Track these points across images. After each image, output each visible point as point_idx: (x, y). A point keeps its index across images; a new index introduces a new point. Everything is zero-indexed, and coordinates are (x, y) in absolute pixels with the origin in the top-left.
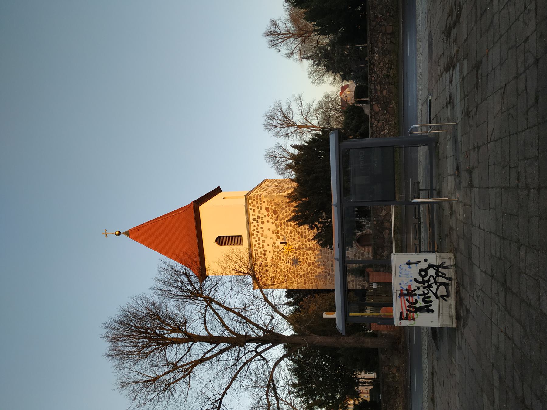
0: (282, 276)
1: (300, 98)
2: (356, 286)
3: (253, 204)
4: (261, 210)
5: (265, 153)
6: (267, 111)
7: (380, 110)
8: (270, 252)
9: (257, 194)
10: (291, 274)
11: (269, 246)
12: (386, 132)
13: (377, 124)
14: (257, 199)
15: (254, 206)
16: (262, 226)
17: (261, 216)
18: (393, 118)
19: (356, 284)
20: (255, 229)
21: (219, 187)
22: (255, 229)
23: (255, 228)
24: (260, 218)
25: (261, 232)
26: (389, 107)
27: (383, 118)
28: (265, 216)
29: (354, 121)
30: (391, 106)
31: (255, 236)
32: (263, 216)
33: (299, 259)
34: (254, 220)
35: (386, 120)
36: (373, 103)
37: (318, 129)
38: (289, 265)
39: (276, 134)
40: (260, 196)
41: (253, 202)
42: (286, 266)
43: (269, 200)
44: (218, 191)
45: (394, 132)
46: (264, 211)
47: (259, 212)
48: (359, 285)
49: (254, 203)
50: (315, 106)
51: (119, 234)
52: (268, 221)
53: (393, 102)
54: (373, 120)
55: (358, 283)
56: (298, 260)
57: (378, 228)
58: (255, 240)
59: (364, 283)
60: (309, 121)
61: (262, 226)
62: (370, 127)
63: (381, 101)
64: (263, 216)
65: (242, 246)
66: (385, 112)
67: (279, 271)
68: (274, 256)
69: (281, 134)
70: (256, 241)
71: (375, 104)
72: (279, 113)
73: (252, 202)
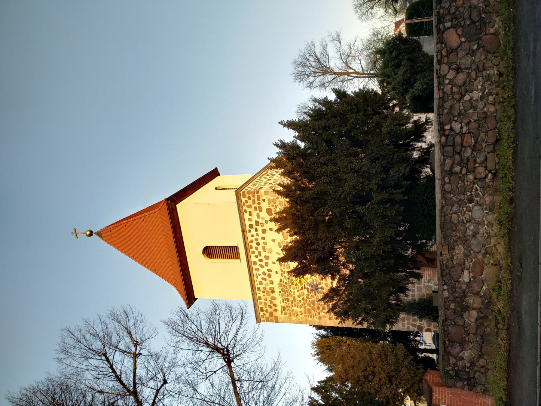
0: (295, 306)
1: (338, 36)
2: (408, 327)
3: (248, 204)
4: (260, 213)
5: (296, 109)
6: (297, 57)
7: (462, 42)
8: (277, 272)
9: (254, 188)
10: (309, 305)
11: (275, 264)
12: (476, 95)
13: (455, 77)
14: (254, 196)
15: (249, 207)
16: (264, 235)
17: (260, 221)
18: (495, 61)
19: (409, 323)
20: (254, 239)
21: (216, 169)
22: (254, 239)
23: (253, 239)
24: (260, 225)
25: (262, 244)
26: (486, 34)
27: (469, 62)
28: (266, 222)
29: (401, 70)
30: (492, 30)
31: (254, 249)
32: (264, 222)
33: (320, 284)
34: (251, 226)
35: (478, 67)
36: (444, 26)
37: (362, 76)
38: (306, 292)
39: (309, 85)
40: (258, 192)
41: (248, 201)
42: (301, 293)
43: (272, 198)
44: (214, 174)
45: (497, 94)
46: (264, 215)
47: (258, 216)
48: (414, 325)
49: (250, 202)
50: (359, 45)
51: (91, 234)
52: (271, 229)
53: (497, 19)
54: (445, 68)
55: (412, 322)
56: (319, 286)
57: (452, 306)
58: (254, 255)
59: (422, 323)
60: (351, 66)
61: (264, 235)
62: (436, 84)
63: (464, 19)
64: (264, 222)
65: (239, 260)
66: (475, 47)
67: (291, 299)
68: (283, 278)
69: (314, 84)
70: (256, 257)
71: (450, 28)
72: (311, 59)
73: (246, 201)
